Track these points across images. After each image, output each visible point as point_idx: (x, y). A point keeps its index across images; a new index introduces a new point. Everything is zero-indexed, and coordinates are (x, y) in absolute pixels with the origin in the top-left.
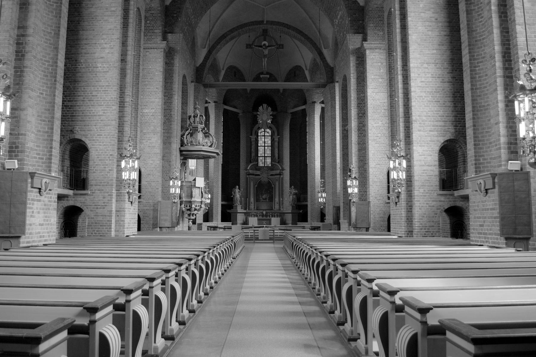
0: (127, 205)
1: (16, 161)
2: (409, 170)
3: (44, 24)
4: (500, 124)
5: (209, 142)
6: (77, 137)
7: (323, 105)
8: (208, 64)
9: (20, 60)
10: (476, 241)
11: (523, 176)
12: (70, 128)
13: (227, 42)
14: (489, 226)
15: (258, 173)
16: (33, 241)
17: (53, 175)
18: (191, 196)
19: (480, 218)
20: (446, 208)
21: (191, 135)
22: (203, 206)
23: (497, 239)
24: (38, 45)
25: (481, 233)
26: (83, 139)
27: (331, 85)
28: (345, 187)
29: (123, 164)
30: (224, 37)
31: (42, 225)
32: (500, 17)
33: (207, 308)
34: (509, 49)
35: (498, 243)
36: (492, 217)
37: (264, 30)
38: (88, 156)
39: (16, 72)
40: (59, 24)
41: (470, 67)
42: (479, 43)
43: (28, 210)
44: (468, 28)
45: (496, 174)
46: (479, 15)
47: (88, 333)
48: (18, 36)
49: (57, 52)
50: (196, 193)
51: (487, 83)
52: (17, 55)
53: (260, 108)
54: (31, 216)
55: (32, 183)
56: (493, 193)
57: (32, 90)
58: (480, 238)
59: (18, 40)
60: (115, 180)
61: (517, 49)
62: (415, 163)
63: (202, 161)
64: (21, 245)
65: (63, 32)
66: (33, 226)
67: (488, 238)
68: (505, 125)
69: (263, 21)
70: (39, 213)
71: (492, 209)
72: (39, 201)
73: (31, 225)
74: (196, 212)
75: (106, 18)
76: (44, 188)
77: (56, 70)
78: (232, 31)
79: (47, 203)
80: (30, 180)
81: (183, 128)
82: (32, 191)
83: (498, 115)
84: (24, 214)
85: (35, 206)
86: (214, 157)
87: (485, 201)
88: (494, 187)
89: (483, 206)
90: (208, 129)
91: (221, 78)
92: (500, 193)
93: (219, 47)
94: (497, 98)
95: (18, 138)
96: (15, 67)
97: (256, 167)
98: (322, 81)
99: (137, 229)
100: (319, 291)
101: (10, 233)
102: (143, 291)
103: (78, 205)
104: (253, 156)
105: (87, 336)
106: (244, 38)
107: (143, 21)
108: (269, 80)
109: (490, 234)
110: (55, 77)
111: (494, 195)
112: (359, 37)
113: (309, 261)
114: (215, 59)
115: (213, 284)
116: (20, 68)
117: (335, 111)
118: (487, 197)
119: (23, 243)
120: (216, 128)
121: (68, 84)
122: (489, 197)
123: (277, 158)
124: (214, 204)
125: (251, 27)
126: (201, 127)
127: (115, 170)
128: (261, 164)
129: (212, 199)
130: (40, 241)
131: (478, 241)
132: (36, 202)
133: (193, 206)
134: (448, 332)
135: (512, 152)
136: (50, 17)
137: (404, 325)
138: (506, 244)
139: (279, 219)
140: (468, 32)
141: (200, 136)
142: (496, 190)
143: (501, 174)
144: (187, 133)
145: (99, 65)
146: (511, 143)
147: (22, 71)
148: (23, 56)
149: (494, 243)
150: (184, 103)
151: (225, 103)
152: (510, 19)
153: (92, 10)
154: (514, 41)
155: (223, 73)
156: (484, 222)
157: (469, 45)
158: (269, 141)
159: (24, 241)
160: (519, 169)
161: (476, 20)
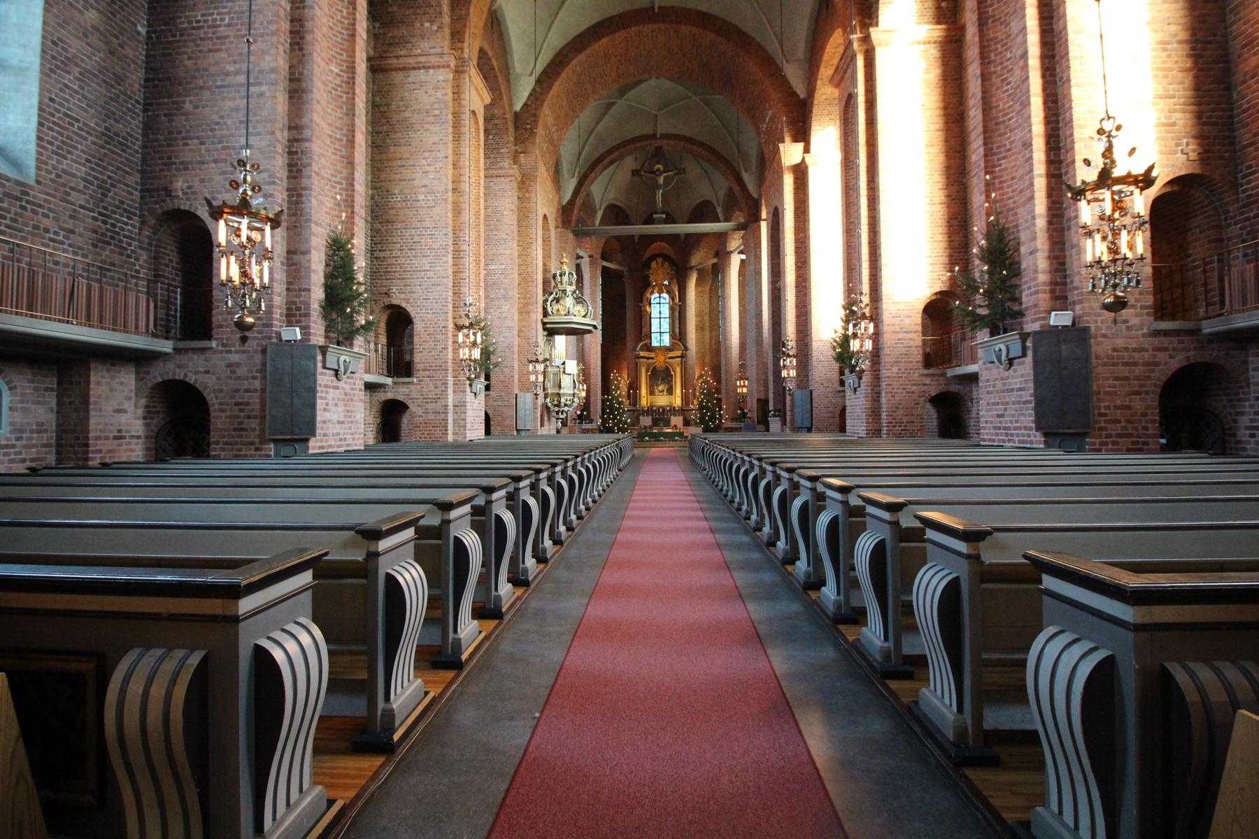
0: (469, 397)
1: (298, 329)
2: (876, 337)
3: (330, 125)
4: (1039, 254)
5: (583, 312)
6: (395, 302)
7: (743, 257)
8: (579, 201)
9: (295, 177)
10: (990, 440)
11: (1078, 333)
12: (385, 290)
13: (605, 168)
14: (1013, 416)
15: (652, 355)
16: (330, 446)
17: (356, 350)
18: (560, 387)
19: (998, 404)
20: (933, 394)
21: (557, 300)
22: (576, 400)
23: (1029, 436)
24: (322, 155)
25: (999, 428)
26: (404, 305)
27: (755, 225)
28: (777, 370)
29: (461, 338)
30: (599, 160)
31: (343, 423)
32: (1043, 76)
33: (581, 539)
34: (1058, 129)
35: (1031, 442)
36: (1019, 403)
37: (657, 148)
38: (412, 330)
39: (290, 196)
40: (353, 125)
41: (986, 167)
42: (1002, 127)
43: (319, 402)
44: (984, 104)
45: (1029, 334)
46: (1003, 81)
47: (365, 577)
48: (289, 141)
49: (353, 169)
50: (567, 382)
51: (1013, 191)
52: (290, 171)
53: (654, 264)
54: (325, 410)
55: (324, 361)
56: (1022, 363)
57: (317, 224)
58: (997, 434)
59: (289, 147)
60: (450, 362)
61: (1072, 127)
62: (885, 328)
63: (573, 338)
64: (311, 451)
65: (361, 139)
66: (327, 425)
67: (1012, 435)
68: (1046, 254)
69: (654, 135)
70: (336, 405)
71: (1019, 389)
72: (337, 388)
73: (324, 422)
74: (566, 409)
75: (427, 126)
76: (342, 369)
77: (353, 196)
78: (610, 151)
79: (348, 391)
80: (319, 358)
81: (546, 291)
82: (322, 374)
83: (1034, 239)
84: (313, 406)
85: (330, 396)
86: (589, 332)
87: (1008, 378)
88: (1024, 355)
89: (1004, 385)
90: (582, 293)
91: (597, 223)
92: (1036, 362)
93: (593, 175)
94: (1033, 211)
95: (299, 296)
96: (288, 190)
97: (649, 348)
98: (742, 220)
99: (483, 432)
100: (747, 512)
101: (293, 433)
102: (472, 507)
103: (400, 398)
104: (643, 331)
105: (363, 581)
106: (629, 163)
107: (788, 408)
108: (666, 221)
109: (1015, 428)
110: (353, 207)
111: (1026, 368)
112: (801, 145)
113: (728, 470)
114: (588, 195)
115: (591, 504)
116: (295, 189)
117: (760, 263)
118: (1011, 372)
119: (314, 448)
120: (593, 285)
121: (378, 226)
122: (1015, 371)
123: (679, 334)
124: (592, 399)
125: (638, 145)
126: (570, 289)
127: (450, 349)
128: (655, 343)
129: (588, 391)
130: (339, 446)
131: (994, 441)
132: (331, 390)
133: (563, 400)
134: (1045, 577)
135: (1057, 298)
136: (338, 114)
137: (925, 564)
138: (1045, 443)
139: (681, 418)
140: (984, 110)
141: (569, 301)
142: (1029, 359)
143: (1035, 333)
144: (551, 298)
145: (421, 197)
146: (1056, 284)
147: (299, 195)
148: (299, 171)
149: (1023, 442)
150: (547, 256)
151: (603, 258)
152: (1061, 79)
153: (407, 114)
154: (1067, 115)
155: (600, 214)
156: (1005, 410)
157: (985, 132)
158: (666, 311)
159: (314, 446)
160: (1070, 323)
161: (998, 89)
